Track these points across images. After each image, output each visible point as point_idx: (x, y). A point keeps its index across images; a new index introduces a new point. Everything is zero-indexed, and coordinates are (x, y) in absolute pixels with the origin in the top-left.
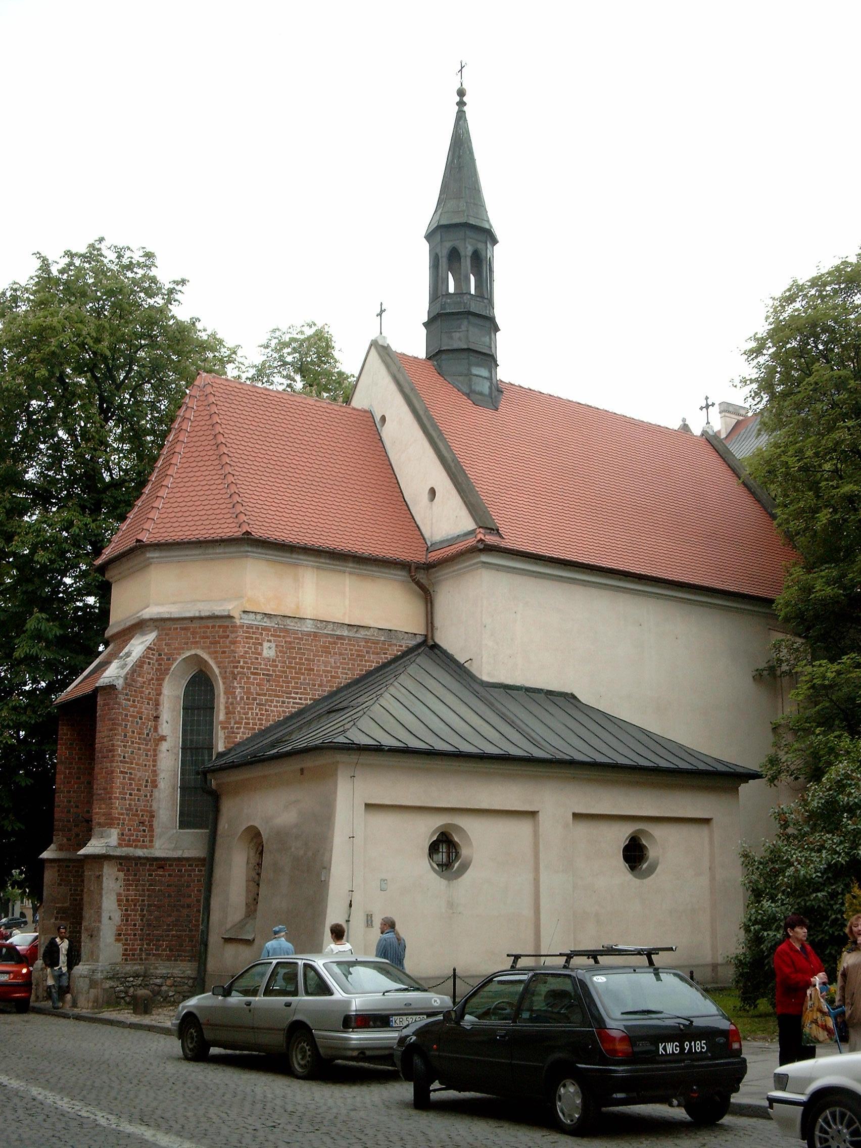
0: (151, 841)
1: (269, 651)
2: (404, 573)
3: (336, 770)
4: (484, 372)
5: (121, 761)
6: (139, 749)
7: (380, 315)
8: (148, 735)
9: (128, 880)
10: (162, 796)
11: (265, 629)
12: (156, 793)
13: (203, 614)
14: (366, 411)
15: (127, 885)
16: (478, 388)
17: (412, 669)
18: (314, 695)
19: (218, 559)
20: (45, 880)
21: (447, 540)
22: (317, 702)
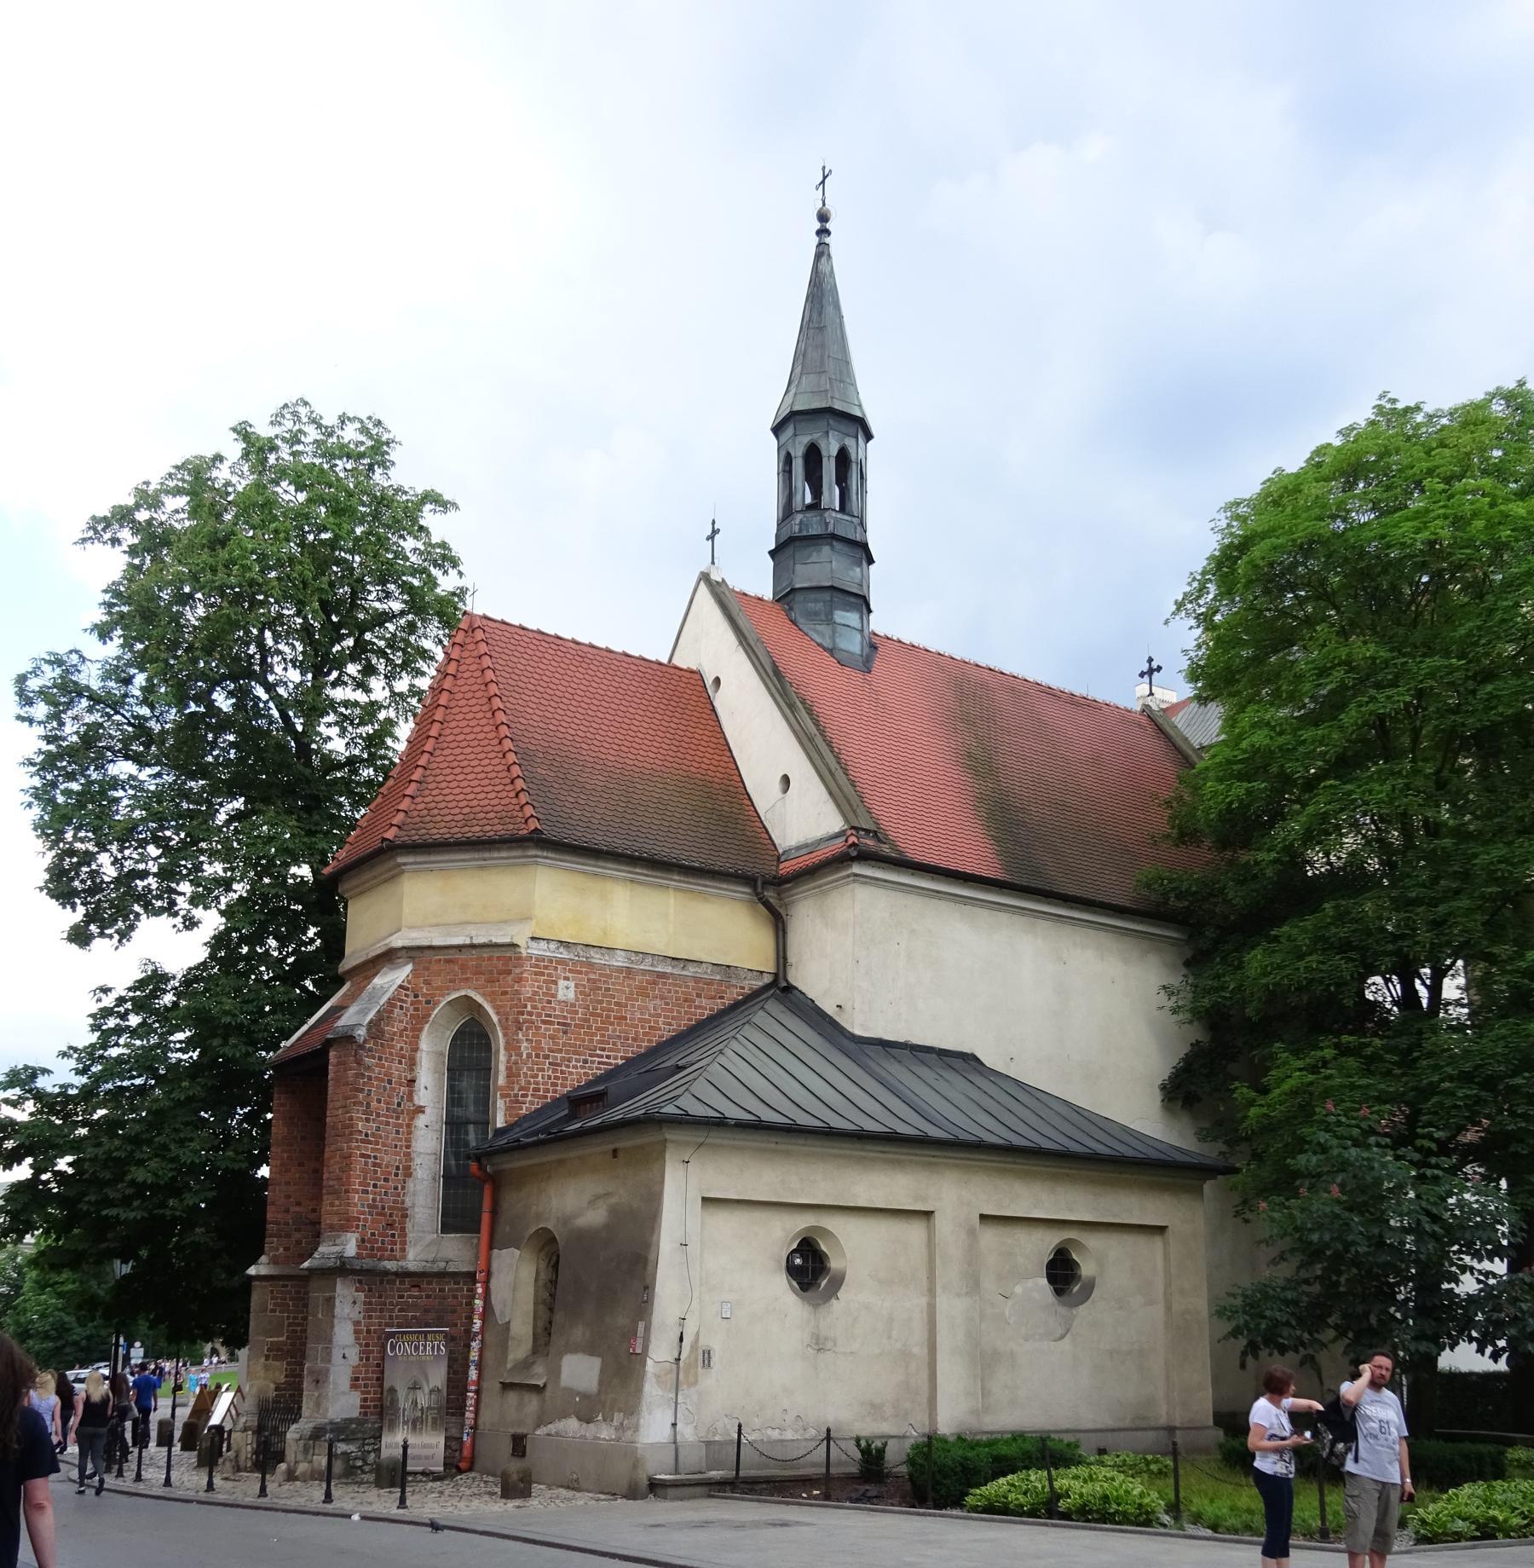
0: (403, 1250)
1: (566, 991)
2: (747, 890)
3: (663, 1152)
4: (852, 618)
5: (363, 1141)
6: (388, 1124)
7: (711, 538)
8: (399, 1105)
9: (370, 1303)
10: (418, 1187)
11: (561, 962)
12: (410, 1184)
13: (476, 941)
14: (692, 672)
15: (369, 1308)
16: (843, 644)
17: (760, 1018)
18: (626, 1051)
19: (496, 866)
20: (252, 1304)
21: (806, 846)
22: (630, 1062)
